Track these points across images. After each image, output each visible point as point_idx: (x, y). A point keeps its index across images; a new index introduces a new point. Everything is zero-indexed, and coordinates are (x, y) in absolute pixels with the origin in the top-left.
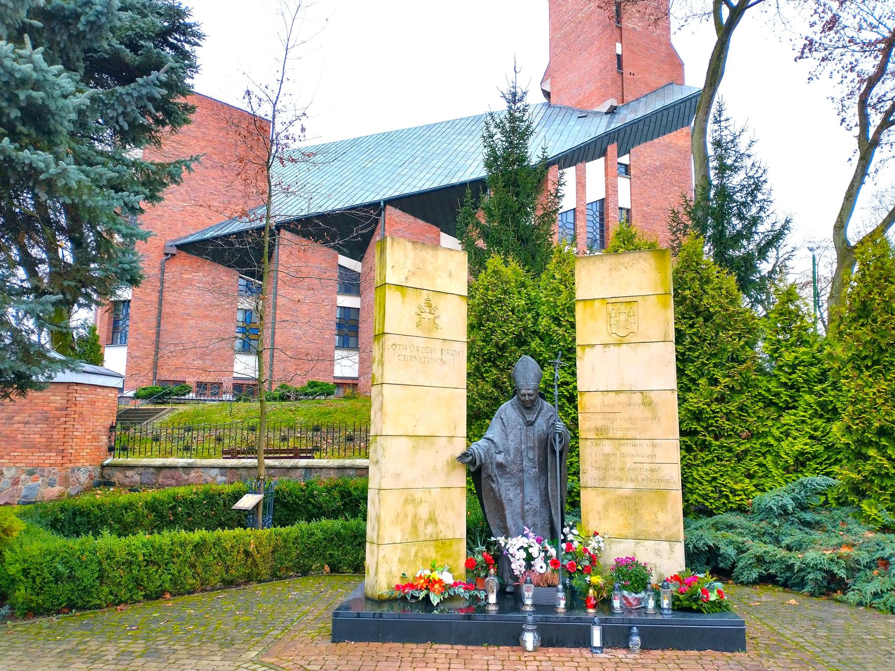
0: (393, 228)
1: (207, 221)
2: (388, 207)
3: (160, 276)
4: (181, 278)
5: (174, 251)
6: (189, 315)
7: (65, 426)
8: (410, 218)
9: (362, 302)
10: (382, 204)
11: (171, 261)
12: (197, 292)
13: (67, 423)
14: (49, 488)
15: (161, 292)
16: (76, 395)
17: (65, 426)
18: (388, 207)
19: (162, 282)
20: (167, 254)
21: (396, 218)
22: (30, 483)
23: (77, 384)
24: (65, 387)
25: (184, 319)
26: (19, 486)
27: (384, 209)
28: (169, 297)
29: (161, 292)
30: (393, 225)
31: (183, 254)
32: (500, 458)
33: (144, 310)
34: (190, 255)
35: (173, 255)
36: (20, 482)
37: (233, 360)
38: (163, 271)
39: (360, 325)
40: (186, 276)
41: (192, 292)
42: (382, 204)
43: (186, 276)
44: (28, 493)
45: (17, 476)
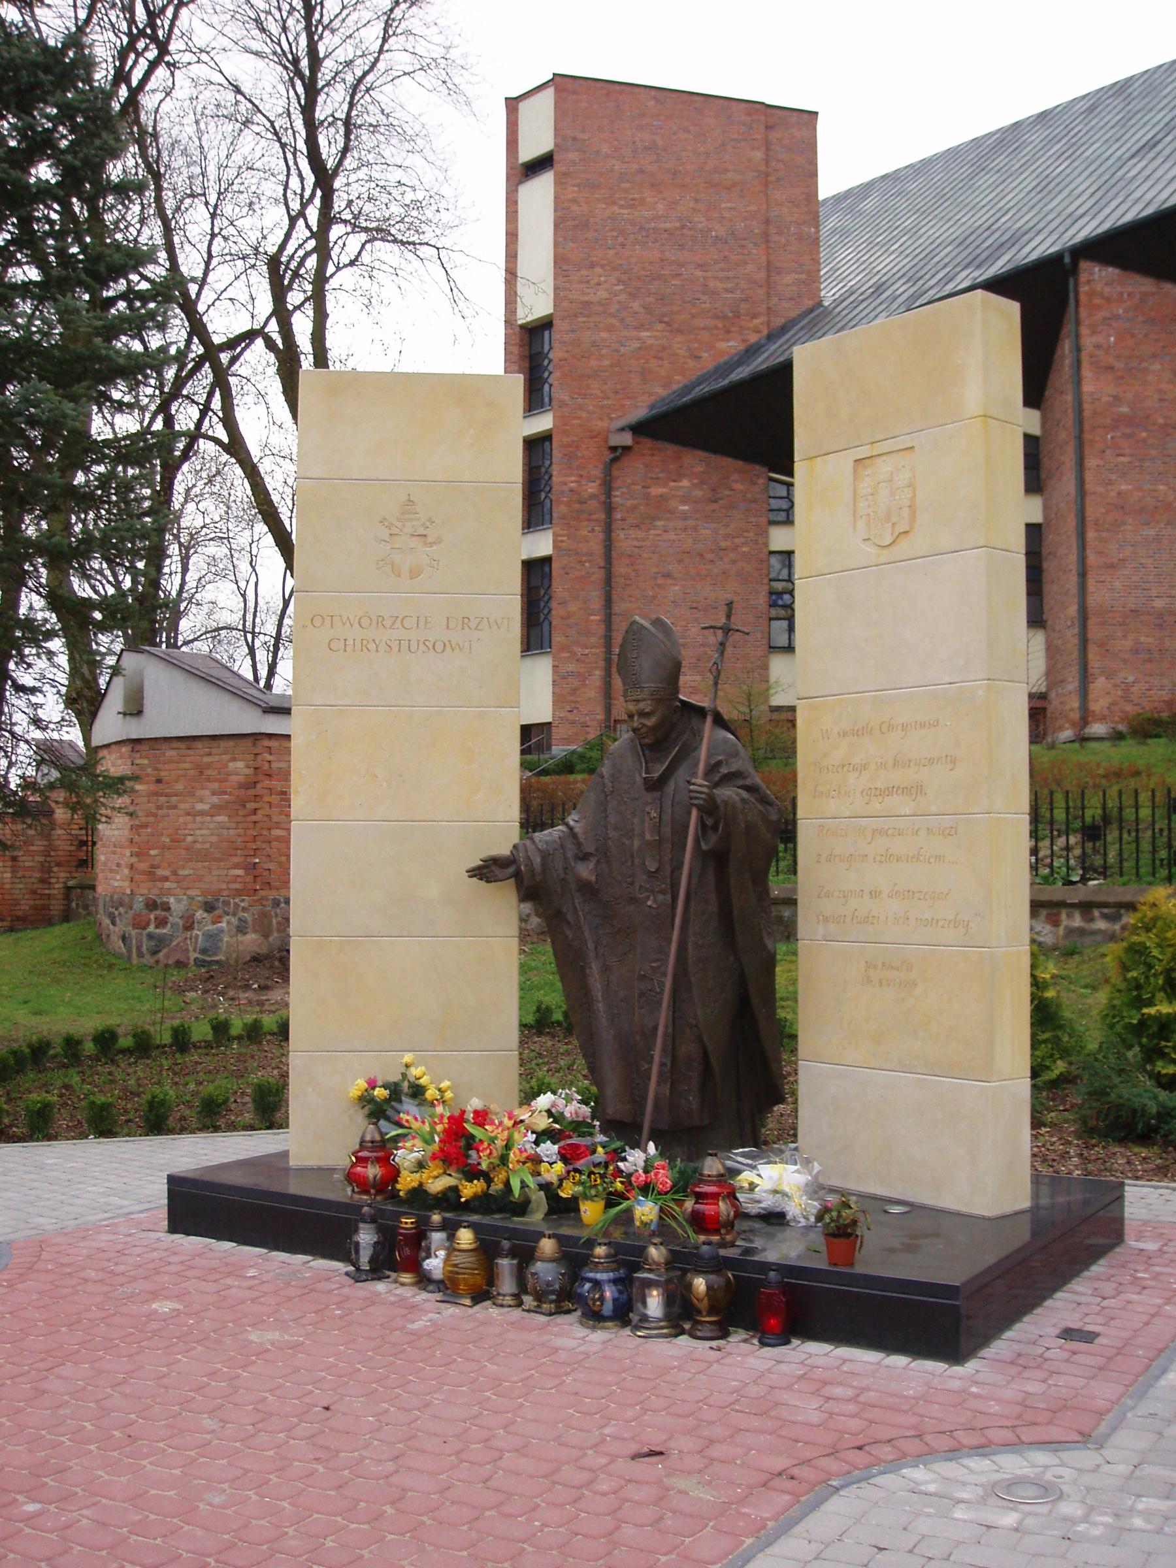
0: (1100, 315)
1: (691, 364)
2: (1084, 265)
3: (603, 498)
4: (647, 497)
5: (627, 439)
6: (668, 575)
7: (253, 818)
8: (1144, 285)
9: (1046, 508)
10: (1067, 260)
11: (625, 462)
12: (680, 524)
13: (259, 812)
14: (240, 938)
15: (608, 530)
16: (269, 757)
17: (253, 818)
18: (1084, 265)
19: (609, 509)
20: (613, 449)
21: (1107, 290)
22: (210, 927)
23: (270, 736)
24: (248, 743)
25: (659, 586)
26: (196, 932)
27: (1074, 270)
28: (625, 539)
29: (608, 530)
30: (1098, 308)
31: (648, 443)
32: (585, 871)
33: (578, 574)
34: (660, 444)
35: (626, 449)
36: (196, 925)
37: (766, 668)
38: (608, 485)
39: (1045, 565)
40: (656, 491)
41: (671, 525)
42: (1067, 260)
43: (656, 491)
44: (208, 944)
45: (191, 912)
